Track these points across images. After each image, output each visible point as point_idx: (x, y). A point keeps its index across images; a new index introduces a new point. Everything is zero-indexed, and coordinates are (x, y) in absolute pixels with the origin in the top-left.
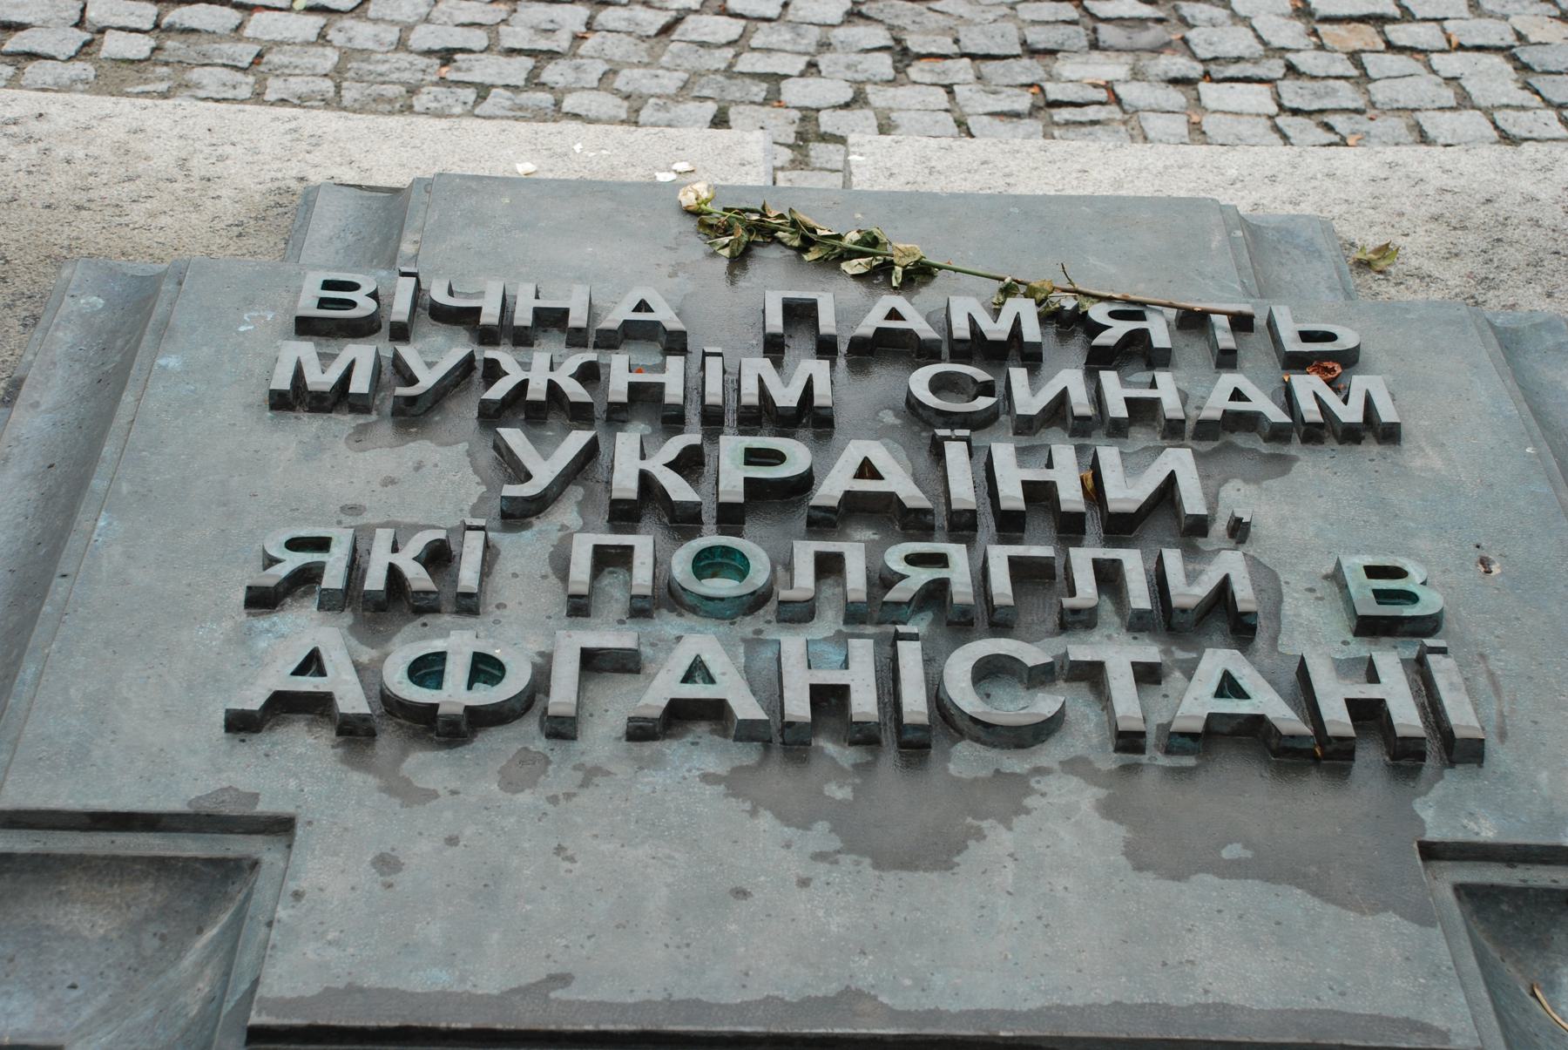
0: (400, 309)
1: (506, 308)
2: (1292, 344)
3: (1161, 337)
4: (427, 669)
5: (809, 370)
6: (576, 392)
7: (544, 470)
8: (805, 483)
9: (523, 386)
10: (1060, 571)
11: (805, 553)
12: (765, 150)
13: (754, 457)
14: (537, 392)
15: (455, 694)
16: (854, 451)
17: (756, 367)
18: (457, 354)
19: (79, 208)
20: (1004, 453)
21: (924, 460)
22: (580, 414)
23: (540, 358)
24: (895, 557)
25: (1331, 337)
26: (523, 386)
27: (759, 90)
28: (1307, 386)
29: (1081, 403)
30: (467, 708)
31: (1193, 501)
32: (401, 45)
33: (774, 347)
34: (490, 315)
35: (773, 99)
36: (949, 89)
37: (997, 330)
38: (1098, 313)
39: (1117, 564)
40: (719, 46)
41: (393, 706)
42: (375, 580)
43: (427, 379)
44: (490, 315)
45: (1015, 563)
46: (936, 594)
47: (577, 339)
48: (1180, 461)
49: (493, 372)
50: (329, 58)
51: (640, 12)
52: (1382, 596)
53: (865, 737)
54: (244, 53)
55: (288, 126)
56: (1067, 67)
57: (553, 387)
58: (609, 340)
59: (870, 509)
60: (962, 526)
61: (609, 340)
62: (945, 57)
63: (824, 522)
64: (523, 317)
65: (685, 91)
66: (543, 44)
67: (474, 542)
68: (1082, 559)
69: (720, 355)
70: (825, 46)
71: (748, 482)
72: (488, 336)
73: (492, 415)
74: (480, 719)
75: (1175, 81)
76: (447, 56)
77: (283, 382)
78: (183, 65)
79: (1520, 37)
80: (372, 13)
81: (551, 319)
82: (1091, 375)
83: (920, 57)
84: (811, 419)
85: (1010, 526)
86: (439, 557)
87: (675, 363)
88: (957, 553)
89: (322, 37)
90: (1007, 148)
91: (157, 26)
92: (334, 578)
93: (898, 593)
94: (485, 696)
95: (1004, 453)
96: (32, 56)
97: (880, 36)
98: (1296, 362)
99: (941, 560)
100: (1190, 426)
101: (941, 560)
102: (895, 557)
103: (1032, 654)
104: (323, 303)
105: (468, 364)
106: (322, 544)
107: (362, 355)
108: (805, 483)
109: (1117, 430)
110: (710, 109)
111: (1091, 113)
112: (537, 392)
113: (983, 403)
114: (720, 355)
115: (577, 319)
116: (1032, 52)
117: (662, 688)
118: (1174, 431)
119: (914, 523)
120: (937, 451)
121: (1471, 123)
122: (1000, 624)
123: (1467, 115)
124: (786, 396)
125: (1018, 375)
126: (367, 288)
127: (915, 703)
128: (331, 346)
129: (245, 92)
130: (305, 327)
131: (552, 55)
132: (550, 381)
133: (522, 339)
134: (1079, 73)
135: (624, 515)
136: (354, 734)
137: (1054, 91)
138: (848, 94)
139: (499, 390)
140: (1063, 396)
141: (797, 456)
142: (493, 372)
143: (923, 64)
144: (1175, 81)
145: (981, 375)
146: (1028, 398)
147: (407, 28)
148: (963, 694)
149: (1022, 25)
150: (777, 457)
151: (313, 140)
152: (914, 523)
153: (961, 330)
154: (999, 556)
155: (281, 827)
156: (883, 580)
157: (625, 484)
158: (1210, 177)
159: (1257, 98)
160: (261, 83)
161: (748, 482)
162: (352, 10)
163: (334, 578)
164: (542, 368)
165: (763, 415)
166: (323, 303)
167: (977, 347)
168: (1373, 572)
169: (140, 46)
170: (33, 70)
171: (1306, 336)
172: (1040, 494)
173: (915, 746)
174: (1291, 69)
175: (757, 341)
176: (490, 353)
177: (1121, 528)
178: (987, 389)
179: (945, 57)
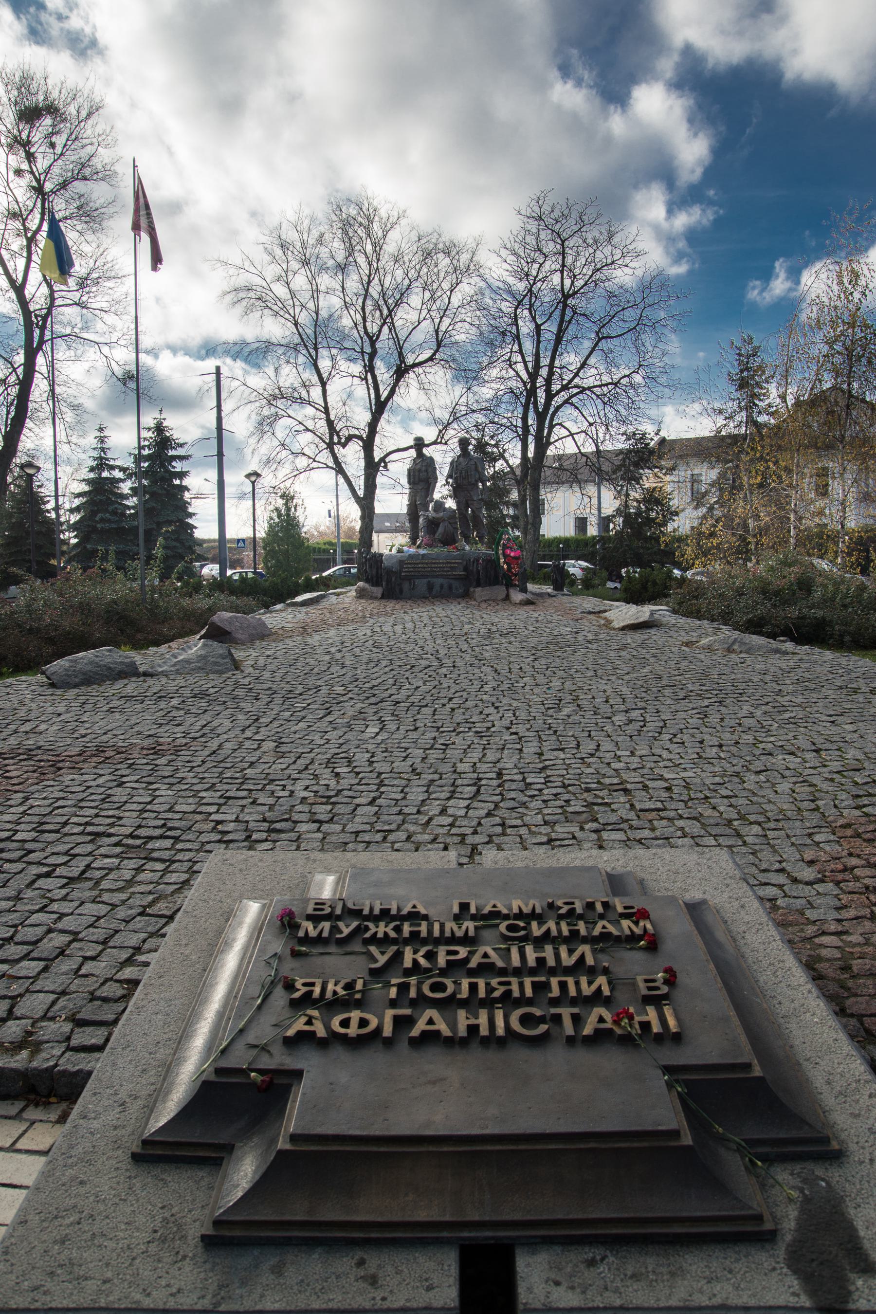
0: (338, 911)
1: (371, 909)
3: (579, 910)
4: (345, 1023)
5: (469, 925)
6: (393, 934)
7: (382, 960)
8: (466, 960)
9: (376, 933)
11: (465, 984)
13: (449, 953)
14: (380, 935)
15: (353, 1031)
16: (482, 949)
17: (450, 925)
18: (355, 924)
20: (529, 949)
22: (394, 941)
23: (382, 924)
24: (494, 982)
25: (632, 908)
26: (376, 933)
27: (457, 839)
29: (554, 932)
31: (590, 961)
32: (343, 831)
33: (457, 918)
34: (366, 912)
35: (462, 842)
36: (520, 836)
38: (559, 903)
41: (334, 1035)
43: (346, 931)
44: (366, 912)
46: (508, 994)
48: (586, 949)
49: (367, 929)
50: (320, 835)
52: (649, 988)
54: (293, 836)
56: (557, 828)
57: (386, 933)
59: (486, 968)
60: (517, 972)
63: (472, 973)
64: (377, 911)
65: (434, 841)
66: (387, 828)
68: (554, 982)
70: (479, 824)
71: (448, 961)
76: (357, 833)
78: (275, 841)
79: (701, 815)
81: (385, 914)
82: (558, 924)
84: (466, 940)
85: (532, 972)
86: (350, 986)
88: (514, 981)
89: (318, 830)
93: (496, 994)
95: (529, 949)
97: (497, 820)
99: (508, 983)
101: (508, 983)
102: (494, 982)
103: (538, 1012)
106: (313, 984)
107: (326, 925)
108: (466, 960)
110: (442, 846)
111: (566, 842)
112: (380, 935)
115: (394, 912)
116: (546, 823)
117: (421, 1026)
118: (585, 940)
119: (503, 972)
121: (687, 841)
122: (530, 1002)
123: (686, 839)
124: (459, 933)
125: (534, 924)
127: (500, 1031)
129: (294, 847)
131: (390, 831)
133: (376, 919)
134: (561, 830)
135: (408, 973)
136: (99, 918)
137: (554, 836)
138: (487, 839)
139: (367, 935)
140: (549, 930)
141: (463, 952)
142: (367, 929)
145: (522, 924)
146: (537, 931)
147: (344, 826)
148: (516, 1025)
149: (544, 815)
150: (456, 953)
152: (503, 972)
154: (528, 982)
156: (490, 989)
157: (408, 963)
159: (620, 836)
161: (448, 961)
164: (382, 929)
165: (453, 940)
166: (315, 910)
167: (520, 915)
168: (646, 981)
169: (264, 835)
170: (231, 845)
171: (625, 908)
172: (541, 961)
173: (501, 1042)
174: (631, 827)
177: (569, 971)
178: (524, 928)
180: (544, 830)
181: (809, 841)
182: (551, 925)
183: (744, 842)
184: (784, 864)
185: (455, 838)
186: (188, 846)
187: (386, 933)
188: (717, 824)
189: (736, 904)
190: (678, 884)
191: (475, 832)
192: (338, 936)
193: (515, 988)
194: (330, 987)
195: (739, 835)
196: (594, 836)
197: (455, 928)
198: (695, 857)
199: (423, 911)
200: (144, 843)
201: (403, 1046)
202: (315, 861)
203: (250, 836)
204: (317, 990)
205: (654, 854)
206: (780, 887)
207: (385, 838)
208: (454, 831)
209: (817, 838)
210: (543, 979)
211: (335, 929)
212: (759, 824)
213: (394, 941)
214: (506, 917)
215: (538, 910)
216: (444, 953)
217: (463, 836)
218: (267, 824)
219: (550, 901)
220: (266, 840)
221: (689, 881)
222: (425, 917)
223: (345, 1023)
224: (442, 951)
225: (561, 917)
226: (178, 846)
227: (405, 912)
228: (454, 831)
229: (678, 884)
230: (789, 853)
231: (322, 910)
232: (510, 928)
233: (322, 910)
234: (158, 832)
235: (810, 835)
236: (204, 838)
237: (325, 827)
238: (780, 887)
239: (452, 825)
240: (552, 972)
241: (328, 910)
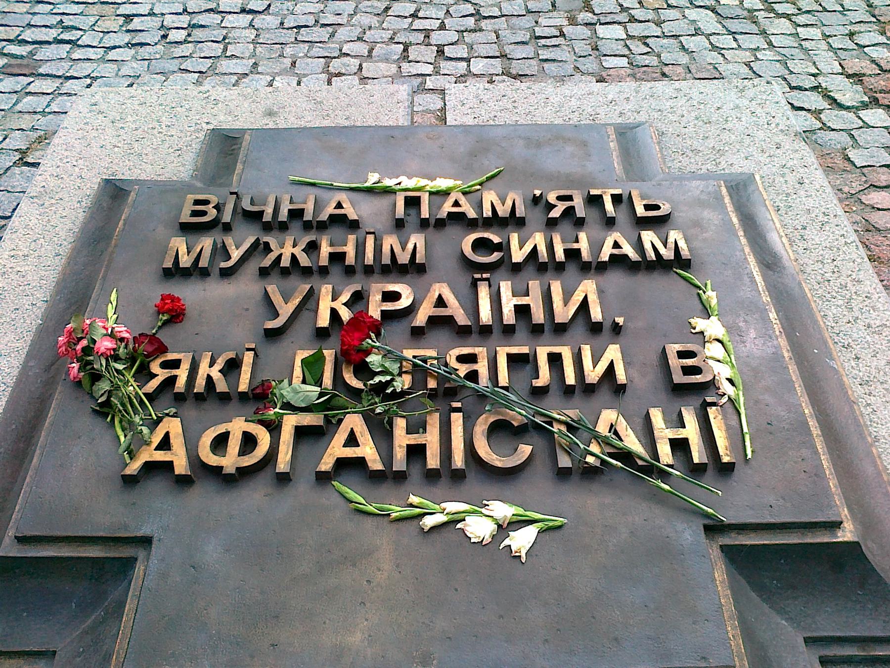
2: (640, 211)
8: (410, 311)
9: (279, 257)
10: (531, 358)
12: (408, 95)
14: (285, 262)
15: (230, 460)
19: (115, 146)
21: (466, 290)
22: (307, 272)
26: (279, 257)
28: (649, 237)
30: (237, 468)
37: (503, 211)
38: (552, 198)
39: (560, 355)
40: (406, 17)
42: (200, 384)
43: (236, 255)
45: (511, 358)
47: (308, 226)
51: (376, 4)
53: (432, 476)
55: (205, 95)
57: (294, 257)
58: (322, 226)
61: (322, 226)
62: (497, 17)
64: (283, 216)
67: (248, 358)
69: (373, 233)
71: (383, 312)
72: (267, 227)
73: (264, 272)
74: (244, 473)
75: (586, 24)
77: (168, 264)
80: (271, 12)
83: (485, 18)
84: (414, 269)
87: (352, 238)
89: (251, 25)
90: (514, 88)
91: (189, 25)
92: (181, 384)
94: (248, 461)
96: (142, 45)
98: (644, 223)
100: (594, 265)
104: (195, 214)
105: (255, 245)
107: (206, 243)
108: (410, 311)
109: (560, 268)
111: (554, 41)
112: (285, 262)
113: (496, 256)
114: (373, 233)
118: (586, 268)
119: (463, 333)
120: (474, 284)
126: (214, 200)
127: (458, 460)
128: (192, 238)
130: (186, 228)
132: (293, 254)
137: (539, 32)
139: (267, 262)
142: (267, 248)
143: (487, 21)
144: (586, 24)
151: (214, 102)
153: (487, 213)
155: (146, 541)
158: (601, 99)
160: (225, 49)
161: (383, 312)
162: (263, 11)
163: (181, 384)
166: (195, 214)
167: (495, 221)
168: (682, 355)
171: (647, 207)
175: (390, 223)
176: (266, 239)
179: (497, 17)
180: (527, 22)
181: (850, 45)
182: (539, 240)
183: (770, 44)
184: (820, 79)
185: (416, 34)
186: (91, 53)
187: (294, 257)
188: (737, 17)
189: (792, 178)
190: (711, 143)
191: (442, 27)
192: (223, 265)
193: (482, 367)
194: (204, 369)
195: (764, 33)
196: (586, 32)
197: (397, 249)
198: (733, 95)
199: (352, 215)
200: (32, 54)
201: (303, 487)
202: (216, 102)
203: (165, 37)
204: (182, 374)
205: (679, 90)
206: (817, 113)
207: (332, 35)
208: (418, 24)
209: (863, 40)
210: (525, 350)
211: (222, 251)
212: (787, 16)
213: (307, 272)
214: (473, 225)
215: (520, 212)
216: (379, 297)
217: (427, 33)
218: (188, 18)
219: (538, 193)
220: (186, 41)
221: (725, 136)
222: (354, 225)
223: (220, 443)
224: (376, 290)
225: (552, 224)
226: (75, 56)
227: (324, 217)
228: (418, 24)
229: (711, 143)
230: (828, 63)
231: (204, 213)
232: (481, 245)
233: (204, 213)
234: (52, 34)
235: (851, 35)
236: (109, 41)
237: (259, 21)
238: (817, 113)
239: (414, 16)
240: (537, 330)
241: (212, 213)
